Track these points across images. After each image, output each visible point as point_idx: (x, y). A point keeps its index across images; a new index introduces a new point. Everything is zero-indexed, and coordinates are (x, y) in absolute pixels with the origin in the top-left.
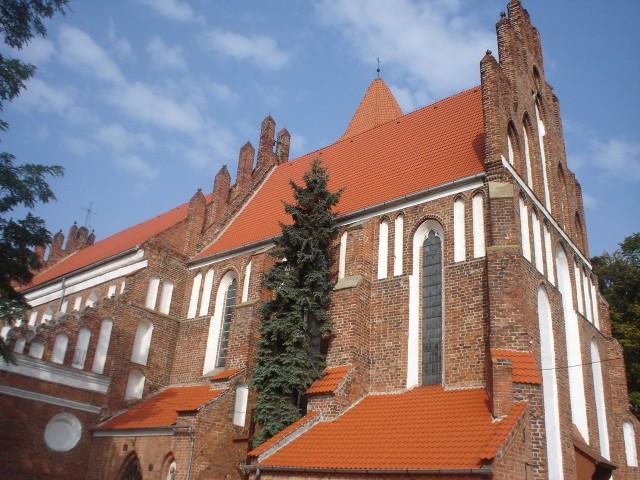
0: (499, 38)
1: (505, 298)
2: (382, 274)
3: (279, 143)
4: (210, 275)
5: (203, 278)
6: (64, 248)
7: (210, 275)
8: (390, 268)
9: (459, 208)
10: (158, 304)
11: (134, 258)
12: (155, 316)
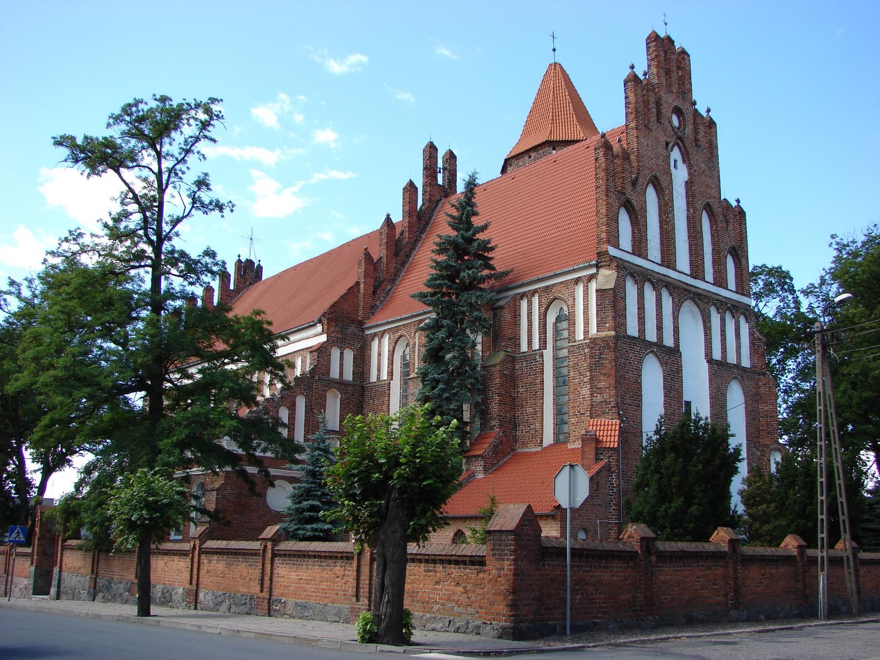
0: (626, 97)
2: (524, 348)
4: (386, 341)
6: (232, 287)
7: (386, 341)
8: (530, 343)
9: (580, 289)
10: (341, 373)
12: (340, 384)
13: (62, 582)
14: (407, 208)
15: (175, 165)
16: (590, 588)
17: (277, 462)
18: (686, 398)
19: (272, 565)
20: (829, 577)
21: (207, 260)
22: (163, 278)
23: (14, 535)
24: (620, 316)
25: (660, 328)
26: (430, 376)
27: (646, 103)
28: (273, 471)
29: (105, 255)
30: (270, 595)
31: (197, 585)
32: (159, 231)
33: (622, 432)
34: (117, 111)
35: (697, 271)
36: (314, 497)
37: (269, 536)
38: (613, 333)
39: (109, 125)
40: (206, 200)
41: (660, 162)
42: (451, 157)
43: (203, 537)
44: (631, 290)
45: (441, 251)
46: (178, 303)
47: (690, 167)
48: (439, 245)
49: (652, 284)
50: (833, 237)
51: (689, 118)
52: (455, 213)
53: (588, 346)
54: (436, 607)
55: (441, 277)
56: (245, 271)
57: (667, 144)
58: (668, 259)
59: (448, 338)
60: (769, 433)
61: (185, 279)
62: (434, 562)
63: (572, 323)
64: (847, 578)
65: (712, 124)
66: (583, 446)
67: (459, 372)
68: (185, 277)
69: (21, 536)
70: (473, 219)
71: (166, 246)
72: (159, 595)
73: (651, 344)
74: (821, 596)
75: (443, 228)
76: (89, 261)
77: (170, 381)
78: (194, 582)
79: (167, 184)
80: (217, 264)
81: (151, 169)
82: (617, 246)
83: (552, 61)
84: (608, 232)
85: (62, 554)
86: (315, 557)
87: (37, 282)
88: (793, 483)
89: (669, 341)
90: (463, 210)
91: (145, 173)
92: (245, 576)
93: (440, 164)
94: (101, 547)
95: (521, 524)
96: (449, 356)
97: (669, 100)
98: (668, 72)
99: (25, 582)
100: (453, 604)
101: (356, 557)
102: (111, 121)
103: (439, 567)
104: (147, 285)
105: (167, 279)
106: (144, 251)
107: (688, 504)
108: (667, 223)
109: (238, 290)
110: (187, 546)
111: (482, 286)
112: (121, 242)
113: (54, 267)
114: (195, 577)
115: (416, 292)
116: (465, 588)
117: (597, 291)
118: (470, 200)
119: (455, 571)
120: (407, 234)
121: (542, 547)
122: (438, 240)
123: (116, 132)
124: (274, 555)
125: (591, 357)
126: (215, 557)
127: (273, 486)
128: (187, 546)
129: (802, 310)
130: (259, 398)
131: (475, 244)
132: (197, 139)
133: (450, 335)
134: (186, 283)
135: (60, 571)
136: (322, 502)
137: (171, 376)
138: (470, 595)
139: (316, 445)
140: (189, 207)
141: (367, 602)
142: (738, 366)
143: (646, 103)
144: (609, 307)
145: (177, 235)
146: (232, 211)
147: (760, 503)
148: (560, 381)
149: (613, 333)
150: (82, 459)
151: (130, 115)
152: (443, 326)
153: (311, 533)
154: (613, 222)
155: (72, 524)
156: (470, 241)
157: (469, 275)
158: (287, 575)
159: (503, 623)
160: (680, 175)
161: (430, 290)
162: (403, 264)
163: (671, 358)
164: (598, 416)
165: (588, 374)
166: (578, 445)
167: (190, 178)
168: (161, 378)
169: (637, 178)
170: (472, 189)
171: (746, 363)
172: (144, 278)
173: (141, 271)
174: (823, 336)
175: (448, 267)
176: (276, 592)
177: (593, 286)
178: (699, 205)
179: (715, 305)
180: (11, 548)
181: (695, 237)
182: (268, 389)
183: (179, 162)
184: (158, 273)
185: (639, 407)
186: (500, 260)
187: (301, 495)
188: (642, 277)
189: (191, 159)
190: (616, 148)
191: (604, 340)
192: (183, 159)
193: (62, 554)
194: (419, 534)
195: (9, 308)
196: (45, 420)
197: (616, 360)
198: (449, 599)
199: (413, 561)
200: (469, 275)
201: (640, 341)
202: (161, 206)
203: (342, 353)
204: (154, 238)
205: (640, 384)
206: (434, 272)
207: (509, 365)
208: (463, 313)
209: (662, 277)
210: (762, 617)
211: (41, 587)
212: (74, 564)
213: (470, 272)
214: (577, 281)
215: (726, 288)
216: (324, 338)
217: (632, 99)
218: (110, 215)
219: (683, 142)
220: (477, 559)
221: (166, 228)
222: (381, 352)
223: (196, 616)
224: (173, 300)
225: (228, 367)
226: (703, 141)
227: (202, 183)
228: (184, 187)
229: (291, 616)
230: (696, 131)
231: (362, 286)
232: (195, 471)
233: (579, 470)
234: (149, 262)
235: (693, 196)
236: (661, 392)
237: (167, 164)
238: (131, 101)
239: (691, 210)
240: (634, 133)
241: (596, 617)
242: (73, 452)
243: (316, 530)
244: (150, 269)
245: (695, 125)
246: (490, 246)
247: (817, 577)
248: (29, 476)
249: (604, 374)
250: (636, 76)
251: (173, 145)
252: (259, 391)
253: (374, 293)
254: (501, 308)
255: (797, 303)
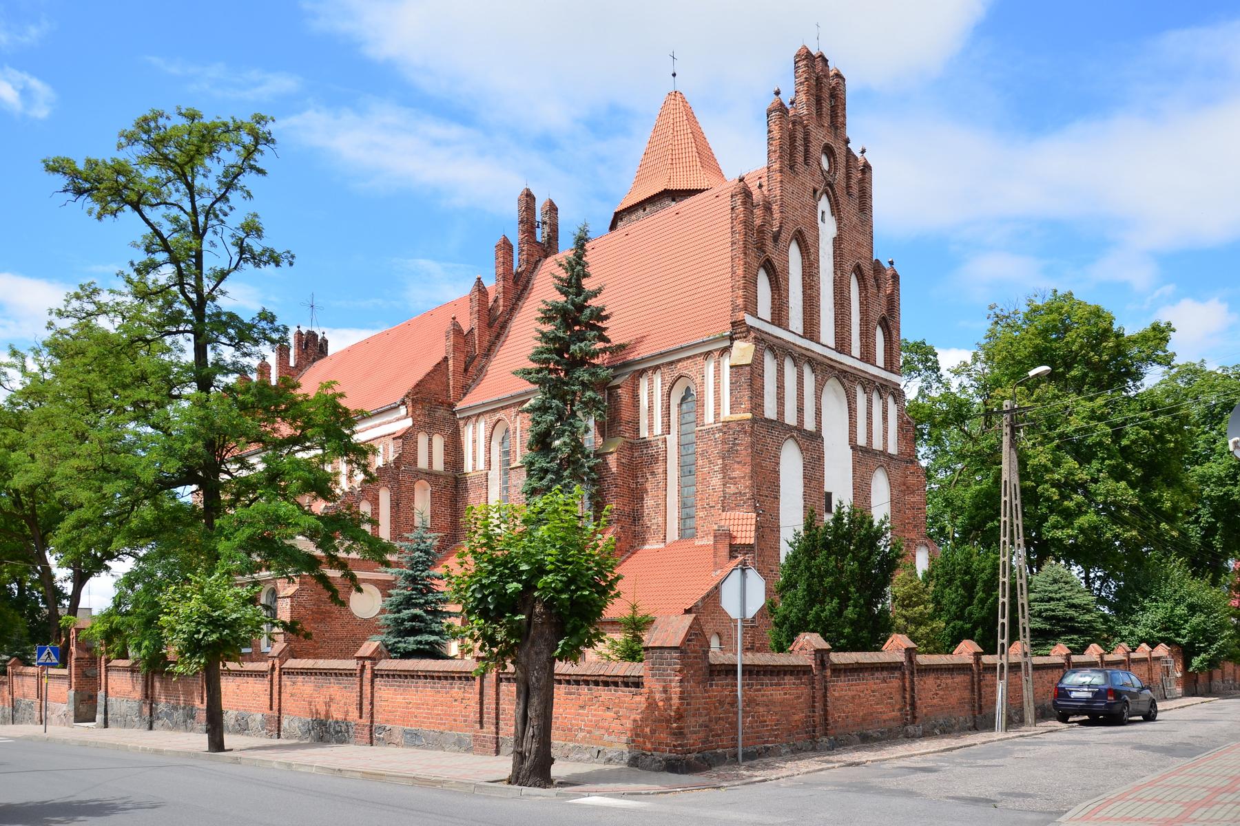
0: (769, 132)
1: (736, 466)
3: (544, 223)
5: (474, 428)
6: (292, 364)
9: (710, 368)
11: (395, 415)
12: (430, 475)
13: (109, 708)
14: (501, 270)
15: (214, 203)
16: (761, 709)
17: (362, 564)
18: (827, 489)
19: (373, 687)
20: (1009, 684)
21: (263, 324)
22: (209, 348)
23: (44, 657)
24: (757, 395)
25: (800, 410)
26: (537, 465)
27: (792, 139)
28: (360, 575)
29: (131, 318)
30: (372, 722)
31: (279, 710)
32: (198, 290)
33: (759, 527)
34: (130, 127)
35: (842, 345)
36: (416, 605)
37: (367, 654)
38: (749, 415)
39: (120, 147)
40: (257, 249)
41: (806, 214)
42: (552, 209)
43: (283, 656)
44: (770, 365)
45: (547, 318)
46: (232, 379)
47: (839, 220)
48: (544, 312)
49: (794, 359)
50: (991, 308)
51: (841, 159)
52: (564, 275)
53: (720, 430)
54: (581, 735)
55: (549, 351)
56: (306, 345)
57: (815, 191)
58: (811, 330)
59: (557, 421)
60: (915, 526)
61: (238, 350)
62: (577, 683)
63: (700, 404)
64: (1024, 686)
65: (867, 168)
66: (715, 542)
67: (571, 461)
68: (237, 347)
69: (53, 657)
70: (584, 282)
71: (209, 309)
72: (233, 722)
73: (790, 428)
74: (999, 706)
75: (545, 289)
76: (108, 324)
77: (228, 472)
78: (275, 707)
79: (205, 231)
80: (277, 330)
81: (182, 208)
82: (754, 314)
83: (672, 90)
84: (746, 298)
85: (106, 676)
86: (426, 677)
87: (45, 352)
88: (950, 581)
89: (810, 425)
90: (573, 270)
91: (175, 212)
92: (341, 700)
93: (538, 218)
94: (155, 668)
95: (688, 639)
96: (557, 443)
97: (820, 137)
98: (819, 102)
99: (64, 708)
100: (603, 731)
101: (478, 678)
102: (123, 140)
103: (584, 689)
104: (189, 357)
105: (214, 349)
106: (181, 313)
107: (843, 605)
108: (811, 288)
109: (299, 368)
110: (264, 666)
111: (595, 361)
112: (151, 301)
113: (63, 332)
114: (276, 702)
115: (519, 367)
116: (617, 713)
117: (731, 367)
118: (580, 258)
119: (604, 693)
120: (501, 302)
121: (711, 665)
122: (543, 307)
123: (132, 155)
124: (374, 676)
125: (724, 442)
126: (300, 678)
127: (360, 590)
128: (264, 666)
129: (953, 390)
130: (338, 491)
131: (587, 312)
132: (241, 171)
133: (560, 418)
134: (238, 354)
135: (106, 695)
136: (426, 612)
137: (228, 466)
138: (624, 721)
139: (415, 546)
140: (236, 259)
141: (493, 729)
142: (884, 453)
143: (792, 139)
144: (745, 386)
145: (222, 293)
146: (291, 264)
147: (917, 604)
148: (687, 470)
149: (749, 415)
150: (122, 566)
151: (147, 132)
152: (551, 408)
153: (414, 647)
154: (750, 284)
155: (117, 644)
156: (580, 308)
157: (581, 349)
158: (390, 697)
159: (667, 755)
160: (828, 229)
161: (536, 366)
162: (498, 336)
163: (811, 442)
164: (732, 509)
165: (720, 462)
166: (709, 541)
167: (235, 220)
168: (215, 468)
169: (779, 232)
170: (583, 245)
171: (893, 449)
172: (184, 349)
173: (180, 337)
174: (1012, 417)
175: (556, 339)
176: (378, 719)
177: (726, 363)
178: (848, 267)
179: (862, 384)
180: (43, 670)
181: (842, 305)
182: (346, 479)
183: (218, 200)
184: (201, 341)
185: (777, 498)
186: (617, 332)
187: (401, 603)
188: (781, 351)
189: (234, 196)
190: (757, 195)
191: (740, 423)
192: (223, 196)
193: (106, 676)
194: (572, 654)
195: (12, 385)
196: (71, 519)
197: (752, 445)
198: (597, 727)
199: (560, 682)
200: (581, 349)
201: (778, 425)
202: (199, 256)
203: (430, 440)
204: (193, 296)
205: (777, 473)
206: (539, 344)
207: (626, 453)
208: (574, 393)
209: (804, 352)
210: (937, 731)
211: (86, 708)
212: (121, 687)
213: (582, 345)
214: (708, 354)
215: (874, 364)
216: (409, 422)
217: (776, 134)
218: (132, 264)
219: (832, 189)
220: (631, 679)
221: (208, 285)
222: (474, 437)
223: (281, 747)
224: (226, 374)
225: (299, 455)
226: (855, 190)
227: (252, 228)
228: (227, 233)
229: (397, 745)
230: (848, 177)
231: (451, 362)
232: (264, 574)
233: (752, 575)
234: (189, 327)
235: (841, 255)
236: (801, 482)
237: (203, 202)
238: (149, 114)
239: (839, 273)
240: (778, 176)
241: (767, 742)
242: (111, 557)
243: (420, 642)
244: (191, 336)
245: (848, 167)
246: (603, 314)
247: (994, 685)
248: (59, 584)
249: (739, 463)
250: (782, 104)
251: (209, 176)
252: (337, 483)
253: (466, 370)
254: (618, 387)
255: (947, 386)
